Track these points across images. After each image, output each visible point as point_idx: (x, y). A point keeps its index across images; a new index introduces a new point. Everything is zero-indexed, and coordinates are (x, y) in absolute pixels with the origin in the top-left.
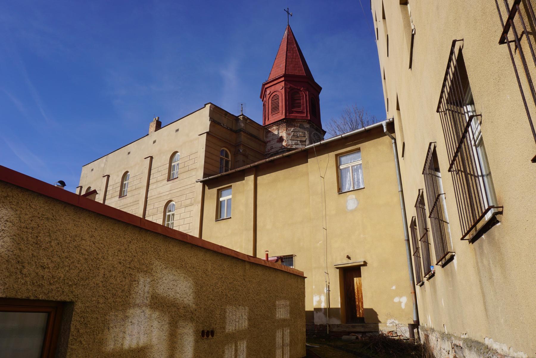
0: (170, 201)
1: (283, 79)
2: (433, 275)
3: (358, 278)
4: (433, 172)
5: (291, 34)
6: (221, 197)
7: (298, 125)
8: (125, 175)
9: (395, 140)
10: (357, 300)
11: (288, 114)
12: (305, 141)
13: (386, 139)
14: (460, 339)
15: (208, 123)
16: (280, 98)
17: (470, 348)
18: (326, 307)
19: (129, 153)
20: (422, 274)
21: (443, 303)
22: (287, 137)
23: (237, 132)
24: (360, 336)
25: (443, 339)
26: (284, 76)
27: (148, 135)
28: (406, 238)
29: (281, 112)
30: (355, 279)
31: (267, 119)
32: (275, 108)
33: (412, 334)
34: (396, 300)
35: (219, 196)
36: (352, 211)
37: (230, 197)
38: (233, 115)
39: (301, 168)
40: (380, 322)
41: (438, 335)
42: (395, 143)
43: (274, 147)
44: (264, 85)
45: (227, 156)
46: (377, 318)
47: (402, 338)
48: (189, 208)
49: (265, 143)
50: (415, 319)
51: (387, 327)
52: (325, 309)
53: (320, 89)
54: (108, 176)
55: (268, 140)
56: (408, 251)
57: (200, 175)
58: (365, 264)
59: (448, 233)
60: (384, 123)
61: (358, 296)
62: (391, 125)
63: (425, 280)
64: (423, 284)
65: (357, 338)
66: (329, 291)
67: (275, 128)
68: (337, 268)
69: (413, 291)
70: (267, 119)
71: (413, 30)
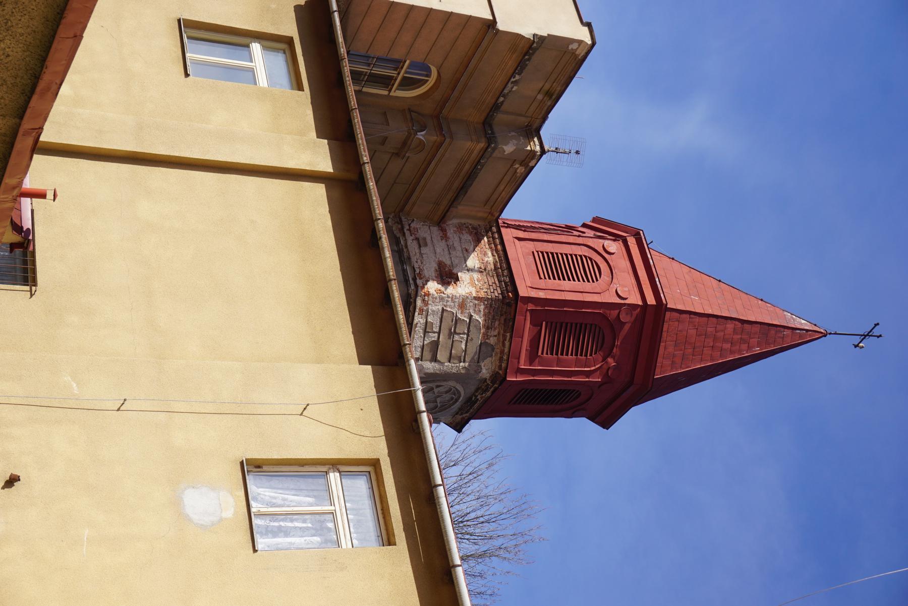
1: (651, 300)
6: (265, 48)
7: (492, 341)
11: (531, 307)
12: (434, 359)
15: (527, 30)
16: (587, 286)
22: (453, 298)
23: (487, 130)
26: (661, 307)
31: (521, 234)
32: (554, 266)
35: (269, 40)
36: (177, 503)
38: (545, 118)
39: (342, 337)
43: (424, 250)
44: (637, 234)
45: (408, 83)
49: (440, 222)
55: (450, 232)
70: (521, 234)
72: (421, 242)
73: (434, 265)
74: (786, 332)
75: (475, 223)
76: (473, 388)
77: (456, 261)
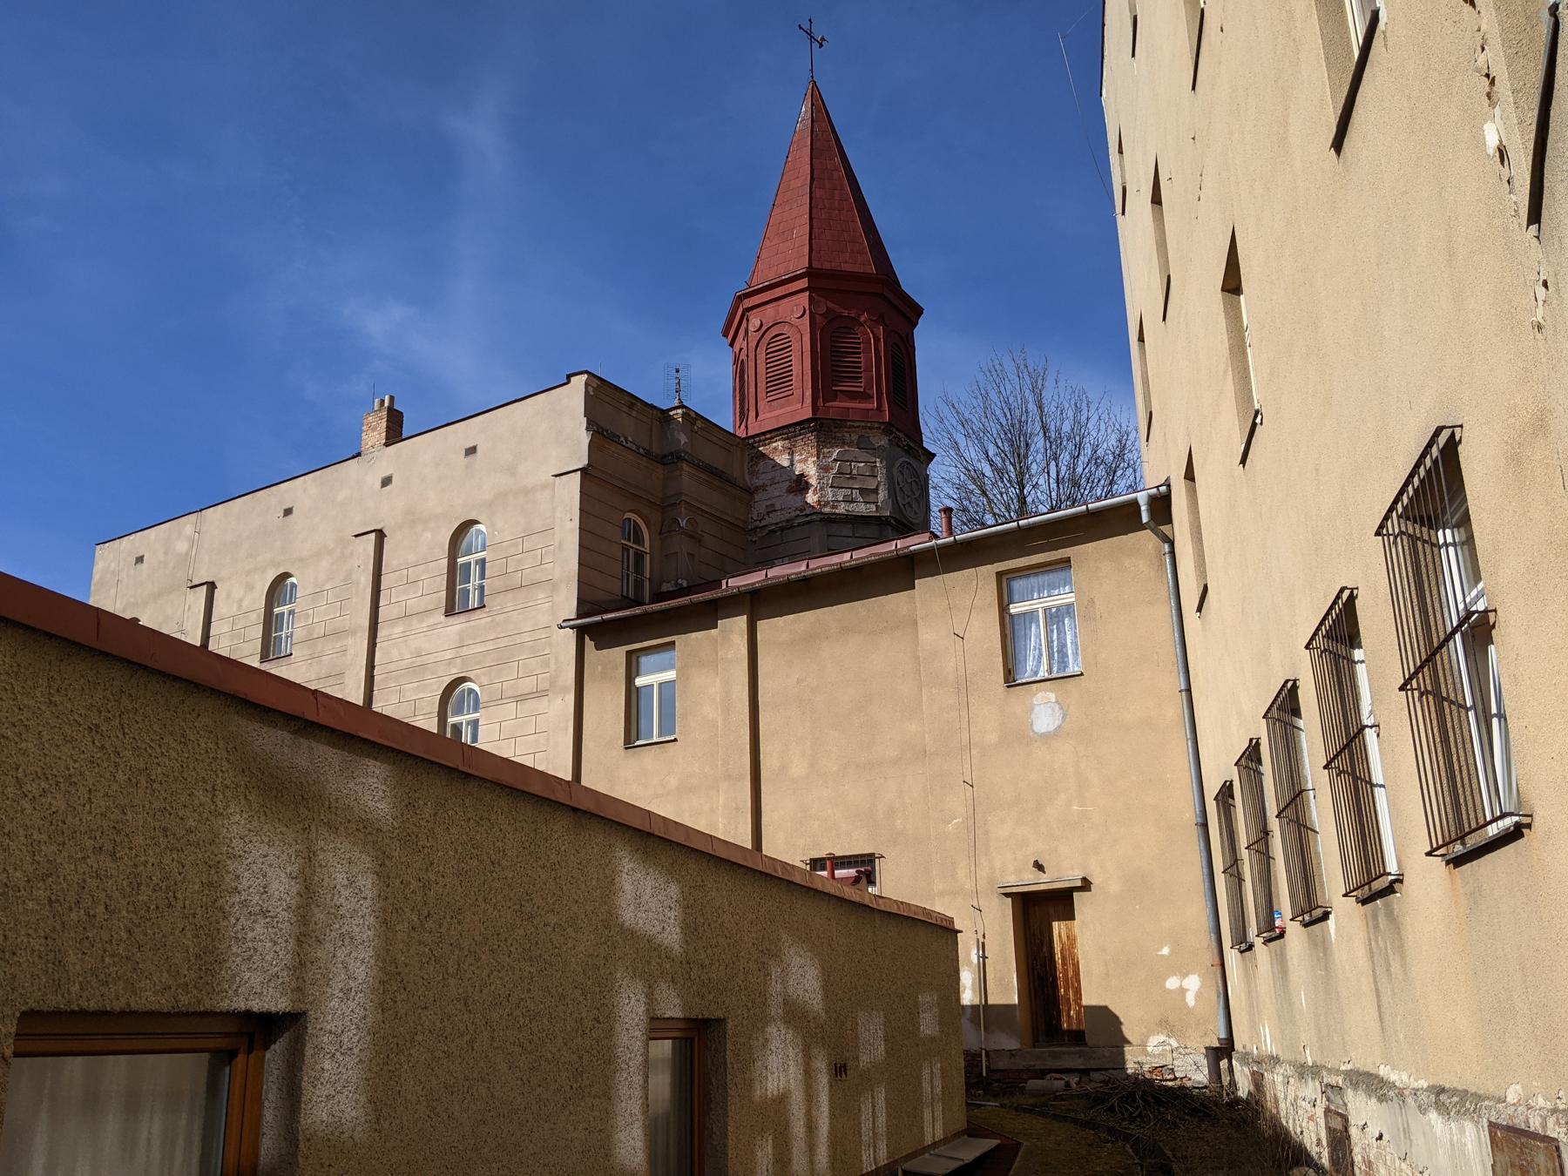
0: (463, 680)
1: (804, 283)
2: (1282, 935)
3: (1063, 924)
4: (1287, 717)
5: (825, 142)
6: (638, 675)
7: (855, 438)
8: (279, 588)
9: (1172, 543)
10: (1061, 983)
11: (820, 403)
12: (876, 491)
13: (1145, 540)
14: (1337, 1072)
15: (584, 438)
16: (796, 347)
17: (1355, 1086)
18: (977, 1002)
19: (288, 512)
20: (1246, 926)
21: (1303, 1000)
22: (820, 478)
23: (669, 460)
24: (1074, 1080)
25: (1301, 1076)
26: (810, 273)
27: (359, 455)
28: (1200, 820)
29: (798, 392)
30: (1055, 924)
31: (752, 414)
32: (779, 381)
33: (1215, 1072)
34: (1172, 983)
35: (632, 671)
36: (1046, 738)
37: (671, 675)
38: (652, 406)
39: (894, 603)
40: (1128, 1042)
41: (1290, 1071)
42: (1172, 552)
43: (778, 507)
44: (741, 298)
45: (638, 539)
46: (1121, 1031)
47: (1189, 1084)
48: (531, 704)
49: (750, 492)
50: (1223, 1035)
51: (1147, 1054)
52: (974, 1007)
53: (919, 311)
54: (211, 586)
55: (758, 482)
56: (1204, 854)
57: (568, 605)
58: (1086, 885)
59: (1317, 854)
60: (1142, 498)
61: (1065, 972)
62: (1162, 505)
63: (1258, 942)
64: (1250, 947)
65: (1068, 1085)
66: (984, 958)
67: (779, 444)
68: (1006, 895)
69: (1217, 961)
70: (752, 414)
71: (1257, 413)
72: (771, 510)
73: (791, 496)
74: (816, 129)
75: (747, 459)
76: (898, 450)
77: (785, 477)
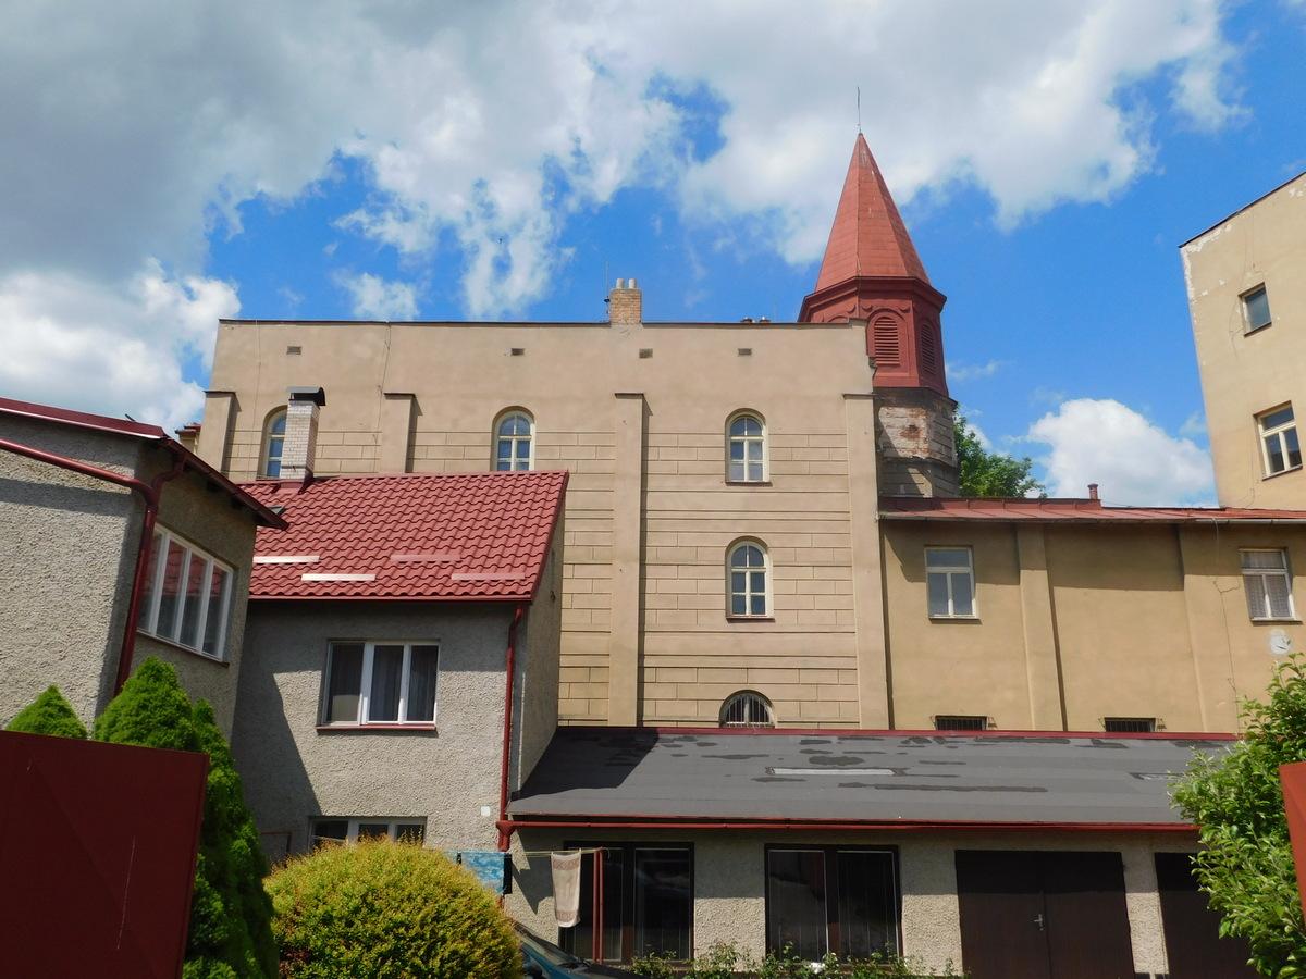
53: (943, 299)
